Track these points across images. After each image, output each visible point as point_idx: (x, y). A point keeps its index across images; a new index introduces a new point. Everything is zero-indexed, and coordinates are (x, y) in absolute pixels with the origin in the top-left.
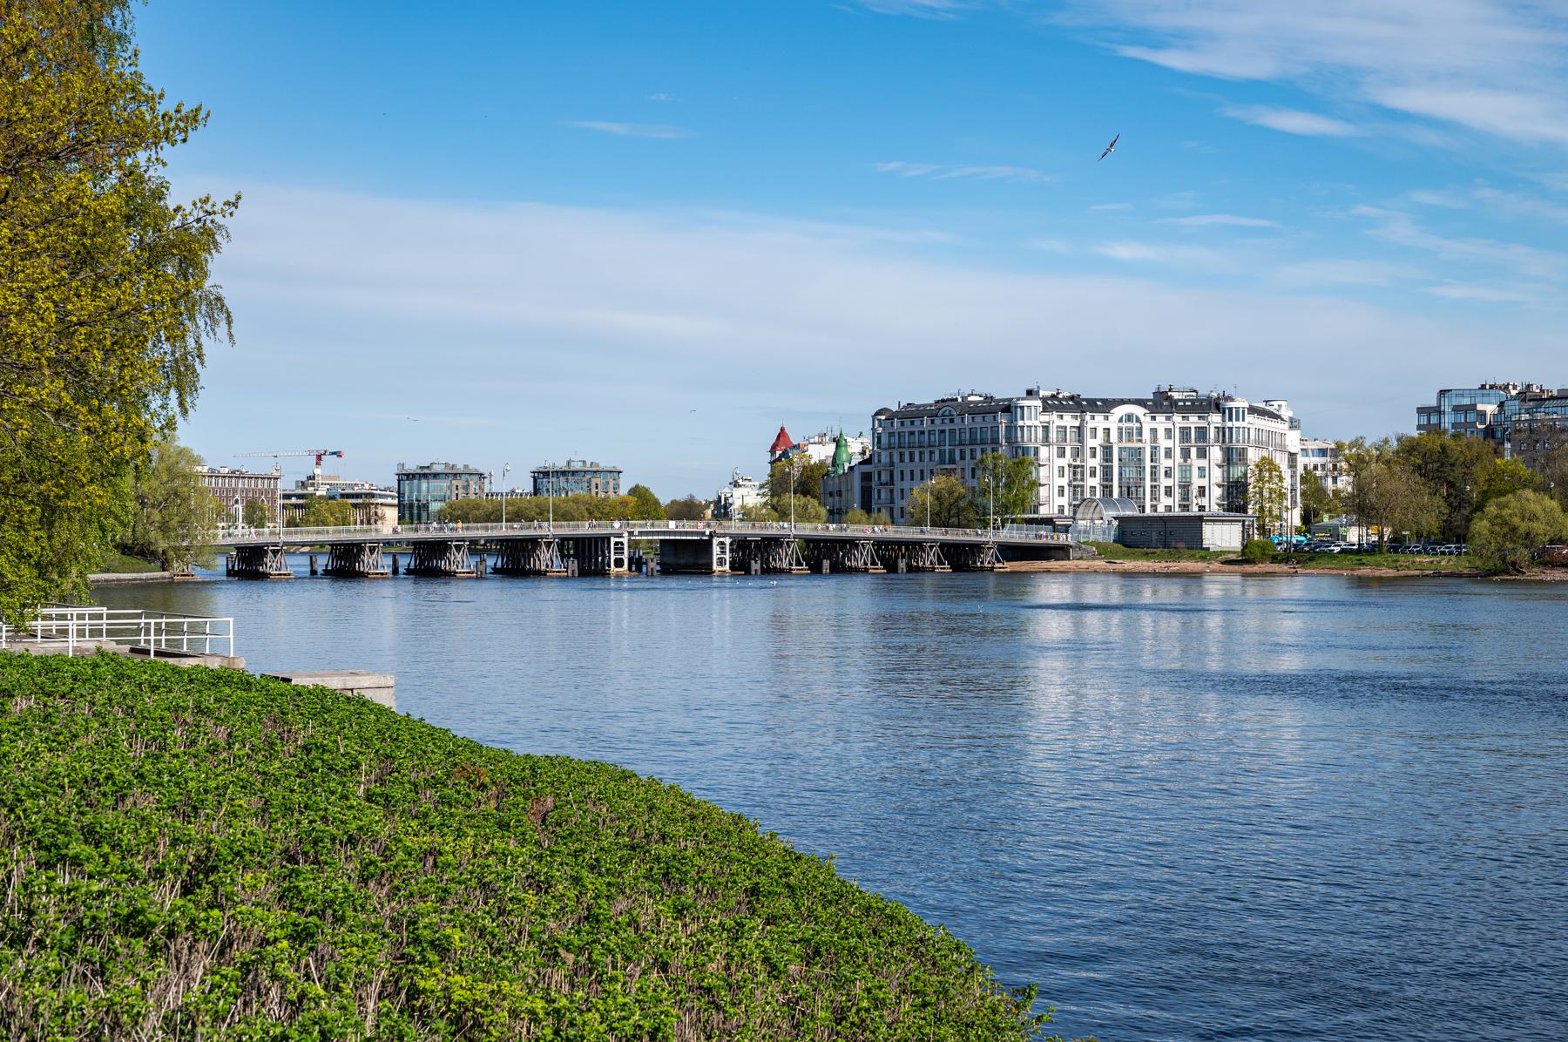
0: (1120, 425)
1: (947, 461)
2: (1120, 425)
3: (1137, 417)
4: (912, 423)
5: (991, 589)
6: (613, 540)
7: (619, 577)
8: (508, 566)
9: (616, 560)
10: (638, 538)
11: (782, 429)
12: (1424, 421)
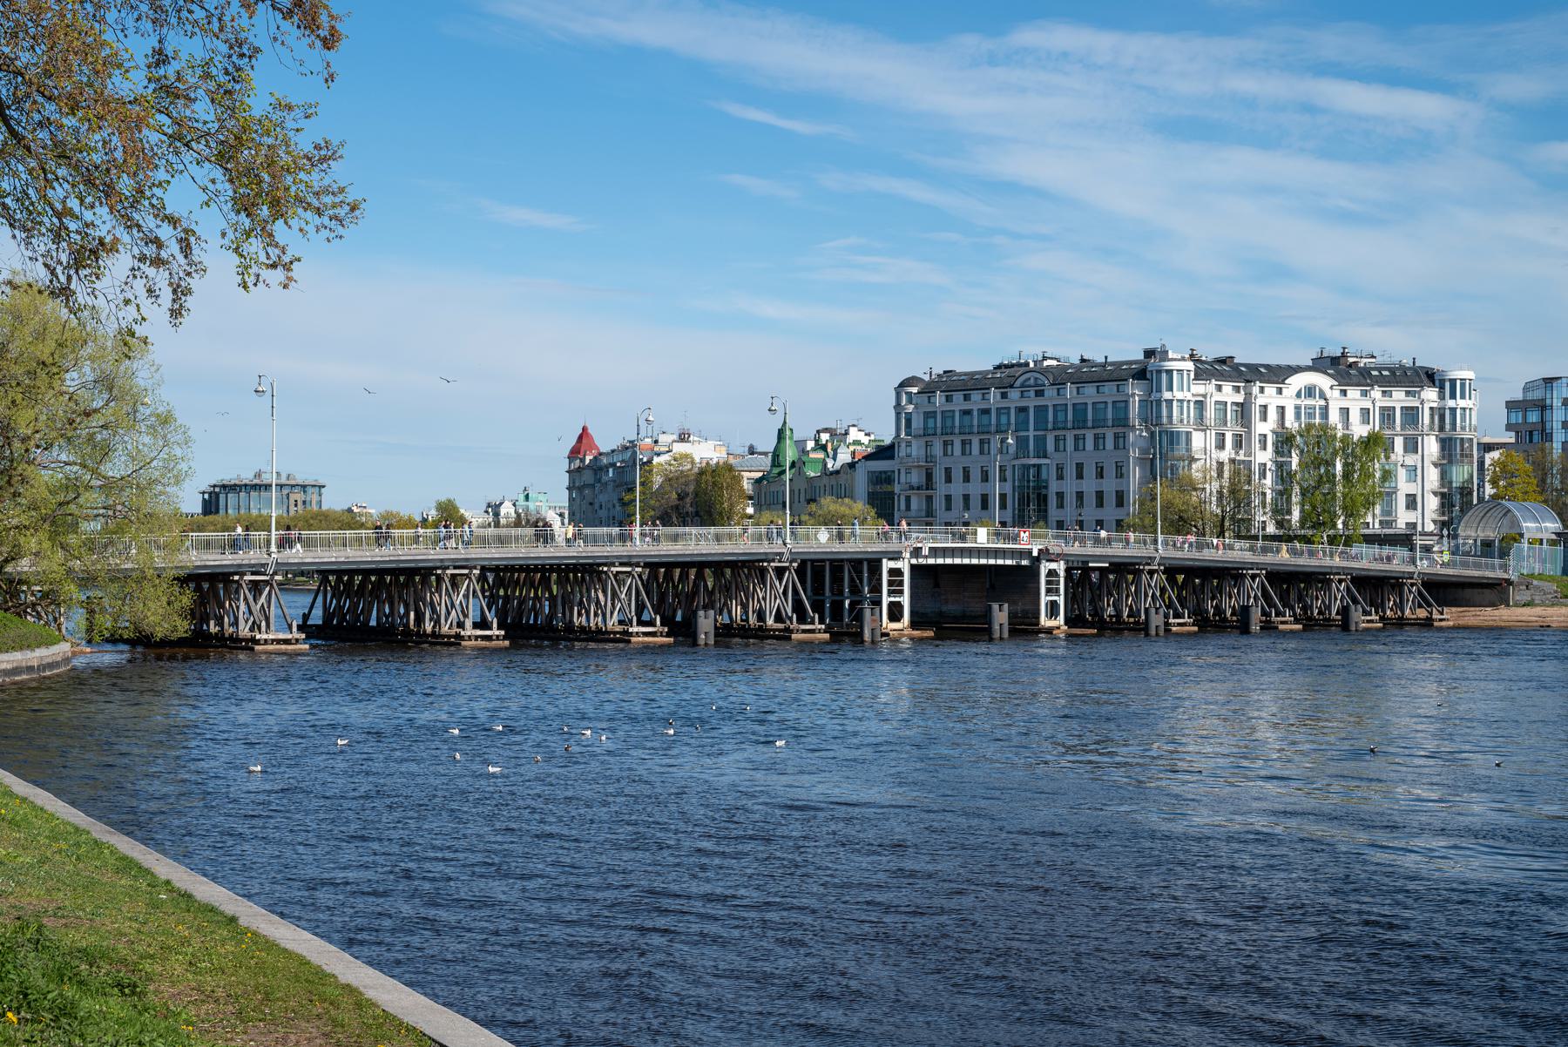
0: (1298, 402)
1: (1031, 454)
2: (1298, 402)
3: (1320, 390)
4: (967, 398)
6: (887, 565)
9: (891, 604)
10: (931, 561)
11: (584, 429)
12: (1517, 418)
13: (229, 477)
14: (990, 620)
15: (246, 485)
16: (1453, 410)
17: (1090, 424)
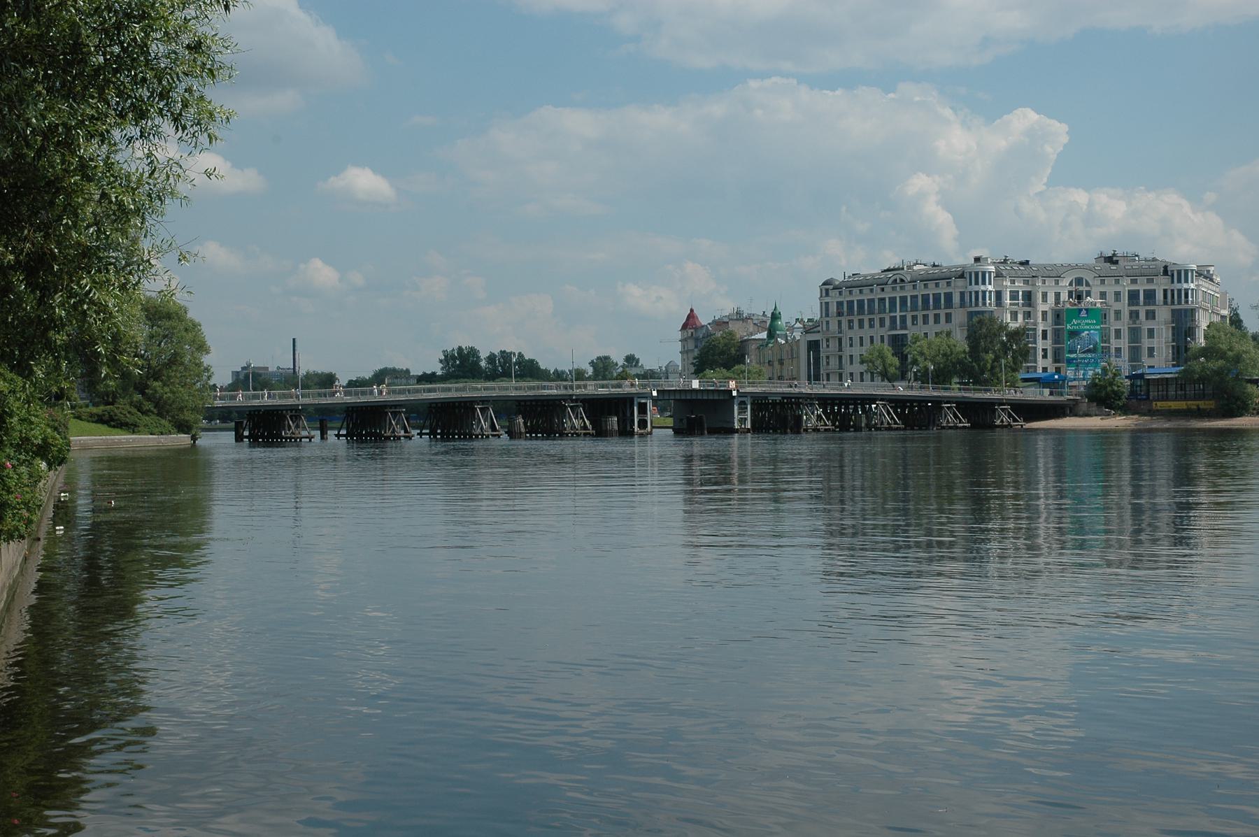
1: (898, 328)
3: (1086, 281)
4: (937, 285)
5: (932, 462)
14: (622, 399)
16: (984, 292)
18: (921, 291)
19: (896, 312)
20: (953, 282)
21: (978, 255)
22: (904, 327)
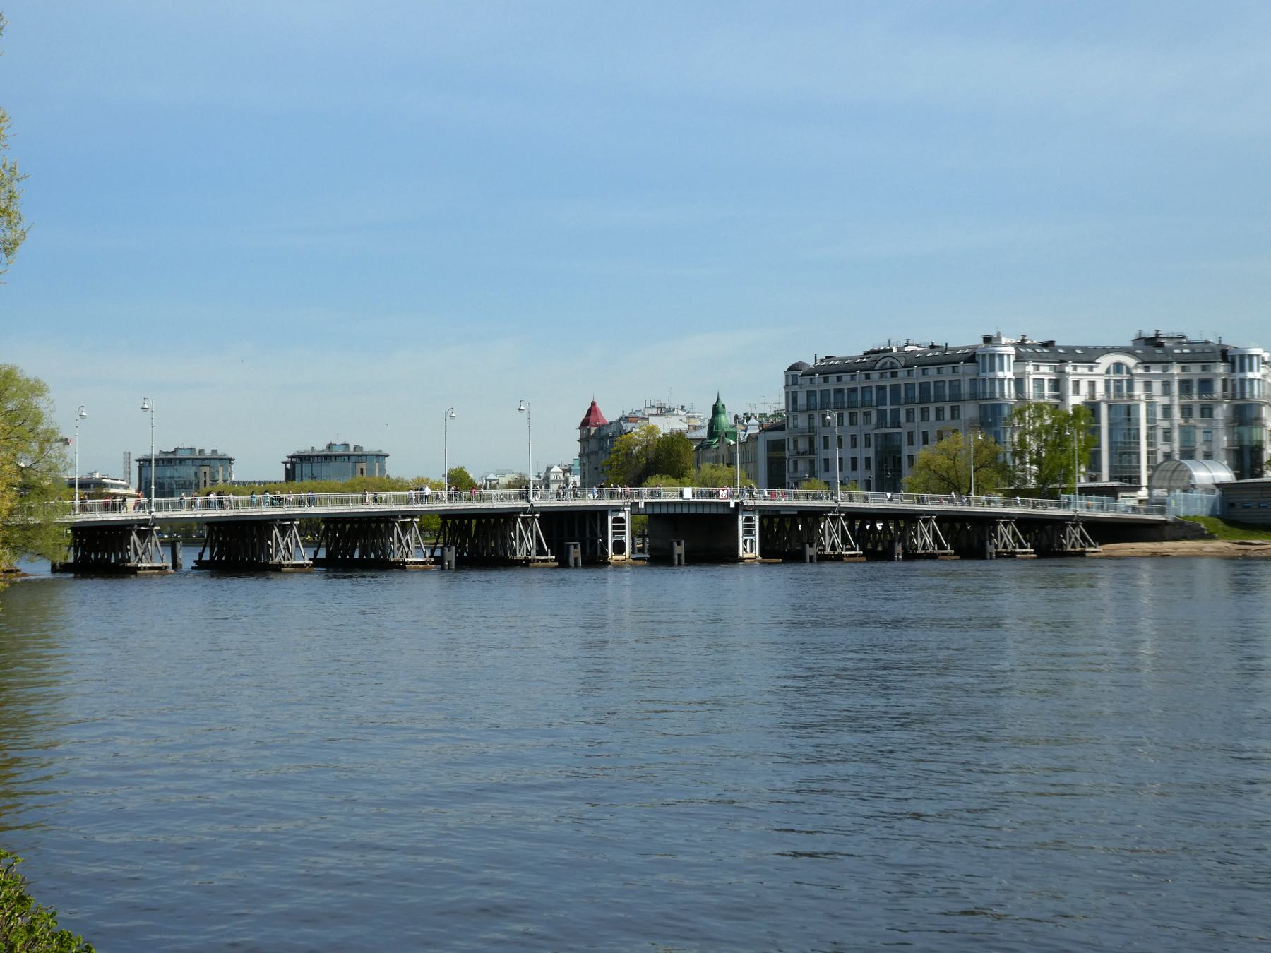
4: (839, 379)
7: (619, 566)
8: (220, 558)
9: (615, 543)
11: (593, 404)
13: (303, 447)
15: (318, 456)
17: (932, 399)
18: (917, 377)
19: (885, 405)
20: (915, 372)
21: (988, 333)
22: (896, 423)
